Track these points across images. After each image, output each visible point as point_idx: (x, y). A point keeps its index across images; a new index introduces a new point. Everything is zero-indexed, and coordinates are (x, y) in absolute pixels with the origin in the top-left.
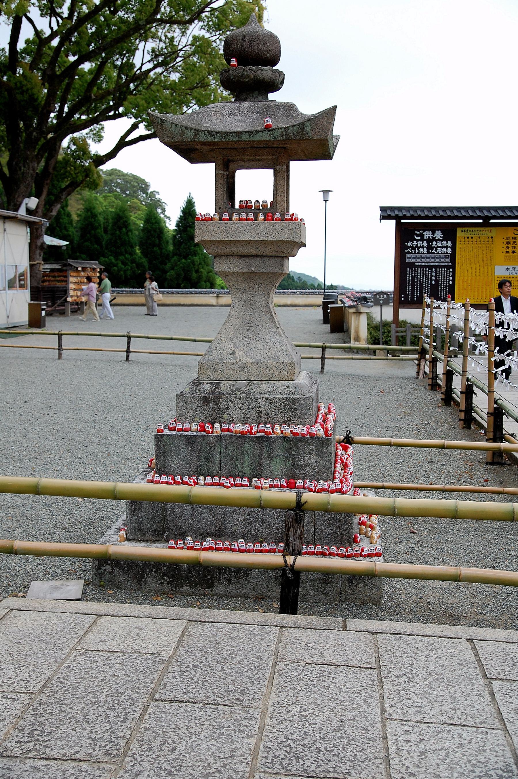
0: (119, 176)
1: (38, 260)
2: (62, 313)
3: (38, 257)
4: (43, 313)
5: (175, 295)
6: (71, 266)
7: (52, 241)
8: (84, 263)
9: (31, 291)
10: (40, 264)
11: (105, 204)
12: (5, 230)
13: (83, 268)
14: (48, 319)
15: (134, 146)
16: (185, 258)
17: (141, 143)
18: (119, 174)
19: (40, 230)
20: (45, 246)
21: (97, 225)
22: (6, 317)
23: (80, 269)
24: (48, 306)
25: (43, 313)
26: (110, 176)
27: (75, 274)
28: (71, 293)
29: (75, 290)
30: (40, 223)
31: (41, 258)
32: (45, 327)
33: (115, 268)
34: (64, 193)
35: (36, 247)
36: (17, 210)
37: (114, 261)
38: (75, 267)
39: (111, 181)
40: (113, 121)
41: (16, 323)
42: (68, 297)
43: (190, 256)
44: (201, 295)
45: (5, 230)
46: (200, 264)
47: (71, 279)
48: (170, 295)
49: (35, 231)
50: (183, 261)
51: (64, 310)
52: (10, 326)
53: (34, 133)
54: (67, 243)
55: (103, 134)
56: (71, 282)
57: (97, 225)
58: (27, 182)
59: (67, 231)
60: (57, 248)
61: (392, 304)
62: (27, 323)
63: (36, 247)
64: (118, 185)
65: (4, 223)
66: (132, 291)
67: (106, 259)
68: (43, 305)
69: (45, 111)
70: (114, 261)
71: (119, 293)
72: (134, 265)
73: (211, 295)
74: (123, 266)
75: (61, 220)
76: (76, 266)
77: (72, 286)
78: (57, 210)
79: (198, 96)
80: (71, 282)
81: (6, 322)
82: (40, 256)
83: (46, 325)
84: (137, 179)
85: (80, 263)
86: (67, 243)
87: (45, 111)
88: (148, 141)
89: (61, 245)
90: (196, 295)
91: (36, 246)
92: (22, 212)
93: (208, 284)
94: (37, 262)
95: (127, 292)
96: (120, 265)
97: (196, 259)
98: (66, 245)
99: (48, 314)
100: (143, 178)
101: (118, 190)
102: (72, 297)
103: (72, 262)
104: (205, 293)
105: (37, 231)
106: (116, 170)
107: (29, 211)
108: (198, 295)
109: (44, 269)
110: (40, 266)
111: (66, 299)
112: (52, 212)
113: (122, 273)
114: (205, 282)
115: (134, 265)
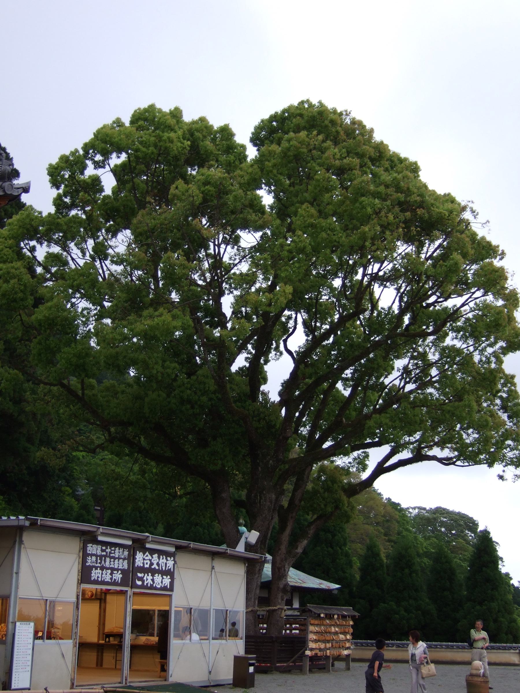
0: (444, 514)
1: (280, 605)
2: (300, 670)
3: (280, 601)
4: (251, 669)
5: (466, 650)
6: (311, 611)
7: (321, 584)
8: (332, 608)
9: (245, 642)
10: (282, 609)
11: (425, 544)
12: (213, 568)
13: (326, 615)
14: (258, 677)
15: (392, 473)
16: (481, 604)
17: (400, 469)
18: (444, 512)
19: (283, 569)
20: (289, 589)
21: (378, 565)
22: (207, 672)
23: (322, 615)
24: (258, 661)
25: (251, 669)
26: (435, 514)
27: (316, 622)
28: (312, 645)
29: (316, 641)
30: (260, 560)
31: (284, 602)
32: (253, 686)
33: (397, 616)
34: (312, 527)
35: (278, 590)
36: (234, 544)
37: (395, 607)
38: (315, 613)
39: (435, 519)
40: (378, 448)
41: (221, 680)
42: (306, 650)
43: (486, 602)
44: (499, 651)
45: (213, 568)
46: (499, 612)
47: (311, 628)
48: (460, 650)
49: (277, 570)
50: (478, 607)
51: (302, 665)
52: (212, 684)
53: (271, 462)
54: (338, 586)
55: (367, 462)
56: (311, 632)
57: (378, 565)
58: (264, 515)
59: (344, 572)
60: (329, 591)
61: (308, 653)
62: (231, 682)
63: (278, 590)
64: (443, 524)
65: (213, 559)
66: (505, 647)
67: (386, 605)
68: (252, 659)
69: (281, 437)
70: (395, 607)
71: (399, 647)
72: (420, 612)
73: (512, 651)
74: (406, 614)
75: (338, 560)
76: (316, 611)
77: (312, 636)
78: (303, 547)
79: (452, 409)
80: (311, 632)
81: (207, 679)
82: (282, 600)
83: (255, 685)
84: (464, 517)
85: (337, 609)
86: (338, 586)
87: (281, 437)
88: (409, 467)
89: (331, 588)
90: (493, 651)
91: (278, 588)
92: (241, 548)
93: (510, 637)
94: (278, 607)
95: (458, 647)
96: (403, 612)
97: (494, 605)
98: (337, 589)
99: (258, 671)
100: (470, 516)
101: (443, 529)
102: (312, 650)
103: (313, 607)
104: (504, 648)
105: (279, 571)
106: (440, 508)
107: (249, 547)
108: (495, 651)
109: (286, 616)
110: (281, 612)
111: (304, 652)
112: (297, 548)
113: (405, 622)
114: (506, 634)
115: (420, 612)
